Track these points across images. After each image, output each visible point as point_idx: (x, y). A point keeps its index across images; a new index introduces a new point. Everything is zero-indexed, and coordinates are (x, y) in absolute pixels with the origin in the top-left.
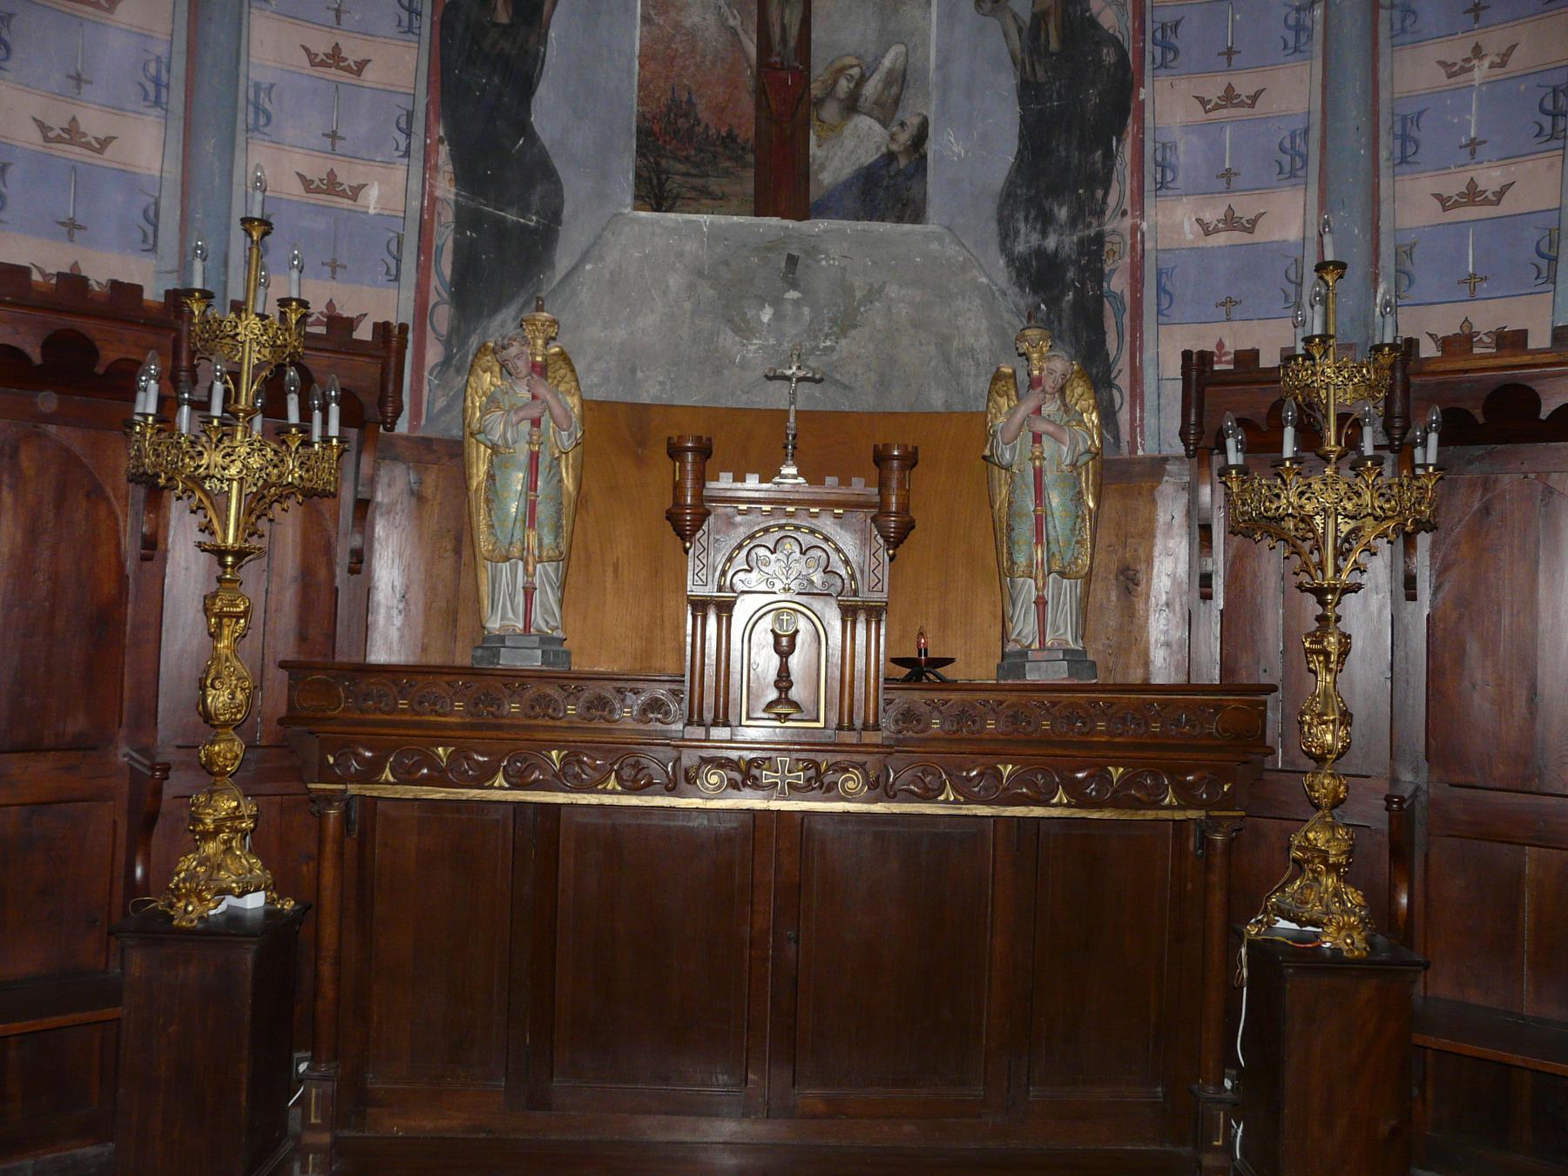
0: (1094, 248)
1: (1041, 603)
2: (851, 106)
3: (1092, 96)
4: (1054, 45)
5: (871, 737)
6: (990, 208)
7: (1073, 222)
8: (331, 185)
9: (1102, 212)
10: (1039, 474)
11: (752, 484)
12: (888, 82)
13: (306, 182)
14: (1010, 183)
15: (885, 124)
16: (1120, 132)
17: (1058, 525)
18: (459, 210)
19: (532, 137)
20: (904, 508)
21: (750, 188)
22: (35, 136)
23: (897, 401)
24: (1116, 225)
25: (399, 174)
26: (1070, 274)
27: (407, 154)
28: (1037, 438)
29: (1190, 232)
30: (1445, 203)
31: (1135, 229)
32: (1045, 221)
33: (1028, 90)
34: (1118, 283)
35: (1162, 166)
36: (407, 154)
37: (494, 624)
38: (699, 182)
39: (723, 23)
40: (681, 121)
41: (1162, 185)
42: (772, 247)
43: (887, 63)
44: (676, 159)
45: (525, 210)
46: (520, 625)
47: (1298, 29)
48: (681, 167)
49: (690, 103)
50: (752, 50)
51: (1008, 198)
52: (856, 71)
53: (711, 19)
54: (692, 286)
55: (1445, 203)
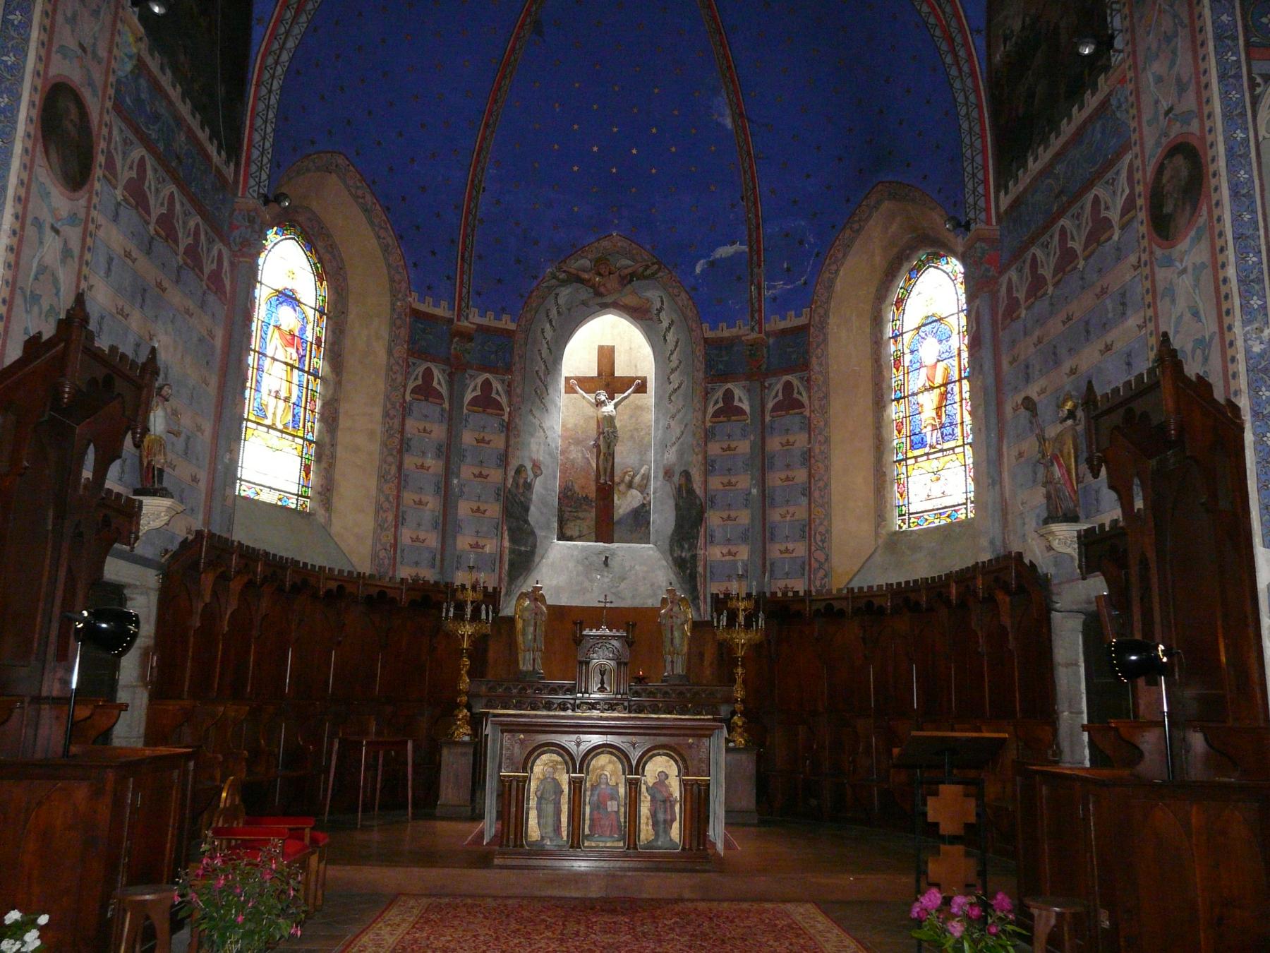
0: (694, 557)
1: (672, 662)
3: (694, 512)
4: (684, 495)
5: (624, 696)
6: (667, 542)
7: (689, 549)
8: (477, 546)
9: (696, 548)
10: (672, 627)
11: (594, 632)
12: (643, 479)
13: (471, 545)
14: (672, 534)
15: (642, 494)
16: (701, 525)
17: (677, 641)
18: (510, 548)
19: (529, 524)
20: (633, 637)
21: (593, 514)
22: (410, 541)
23: (637, 603)
25: (495, 541)
26: (689, 565)
27: (497, 535)
28: (672, 617)
29: (719, 555)
30: (781, 552)
31: (704, 554)
32: (682, 548)
34: (700, 569)
35: (712, 536)
36: (497, 535)
37: (522, 667)
38: (576, 514)
39: (584, 457)
40: (569, 493)
41: (712, 542)
42: (600, 553)
43: (642, 471)
44: (567, 506)
45: (525, 545)
46: (531, 669)
47: (747, 500)
48: (569, 509)
49: (572, 486)
50: (595, 466)
52: (631, 473)
53: (580, 455)
54: (575, 566)
55: (781, 552)
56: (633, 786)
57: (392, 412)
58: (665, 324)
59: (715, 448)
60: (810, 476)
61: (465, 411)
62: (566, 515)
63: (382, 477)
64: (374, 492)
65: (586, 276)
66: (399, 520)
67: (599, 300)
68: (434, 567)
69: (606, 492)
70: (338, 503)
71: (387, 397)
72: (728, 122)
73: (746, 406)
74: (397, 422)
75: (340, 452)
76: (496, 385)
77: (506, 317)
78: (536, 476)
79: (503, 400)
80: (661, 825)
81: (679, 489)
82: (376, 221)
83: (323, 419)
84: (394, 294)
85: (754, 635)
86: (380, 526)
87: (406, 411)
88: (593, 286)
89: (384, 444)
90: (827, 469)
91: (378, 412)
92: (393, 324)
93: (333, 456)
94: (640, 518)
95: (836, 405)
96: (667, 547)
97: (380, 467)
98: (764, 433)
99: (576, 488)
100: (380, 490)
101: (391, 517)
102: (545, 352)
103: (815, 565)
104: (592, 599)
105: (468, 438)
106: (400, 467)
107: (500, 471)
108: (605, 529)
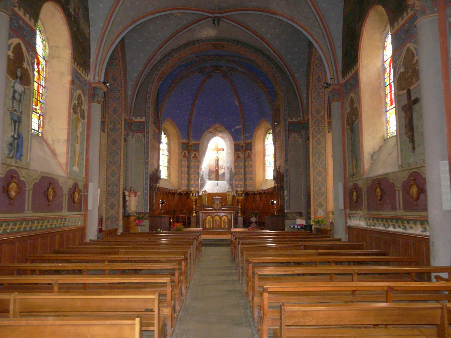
0: (233, 183)
2: (222, 168)
24: (234, 183)
33: (230, 174)
56: (221, 220)
62: (210, 174)
63: (178, 172)
66: (182, 180)
68: (50, 117)
69: (217, 171)
70: (171, 177)
71: (178, 158)
72: (237, 104)
73: (241, 156)
74: (180, 163)
75: (171, 168)
76: (197, 154)
77: (198, 141)
79: (198, 156)
80: (225, 225)
81: (230, 171)
83: (168, 163)
85: (242, 198)
87: (181, 160)
90: (255, 168)
91: (177, 161)
94: (224, 174)
95: (257, 157)
98: (245, 161)
100: (178, 174)
101: (180, 179)
102: (205, 146)
104: (215, 191)
105: (192, 164)
106: (181, 170)
108: (217, 178)
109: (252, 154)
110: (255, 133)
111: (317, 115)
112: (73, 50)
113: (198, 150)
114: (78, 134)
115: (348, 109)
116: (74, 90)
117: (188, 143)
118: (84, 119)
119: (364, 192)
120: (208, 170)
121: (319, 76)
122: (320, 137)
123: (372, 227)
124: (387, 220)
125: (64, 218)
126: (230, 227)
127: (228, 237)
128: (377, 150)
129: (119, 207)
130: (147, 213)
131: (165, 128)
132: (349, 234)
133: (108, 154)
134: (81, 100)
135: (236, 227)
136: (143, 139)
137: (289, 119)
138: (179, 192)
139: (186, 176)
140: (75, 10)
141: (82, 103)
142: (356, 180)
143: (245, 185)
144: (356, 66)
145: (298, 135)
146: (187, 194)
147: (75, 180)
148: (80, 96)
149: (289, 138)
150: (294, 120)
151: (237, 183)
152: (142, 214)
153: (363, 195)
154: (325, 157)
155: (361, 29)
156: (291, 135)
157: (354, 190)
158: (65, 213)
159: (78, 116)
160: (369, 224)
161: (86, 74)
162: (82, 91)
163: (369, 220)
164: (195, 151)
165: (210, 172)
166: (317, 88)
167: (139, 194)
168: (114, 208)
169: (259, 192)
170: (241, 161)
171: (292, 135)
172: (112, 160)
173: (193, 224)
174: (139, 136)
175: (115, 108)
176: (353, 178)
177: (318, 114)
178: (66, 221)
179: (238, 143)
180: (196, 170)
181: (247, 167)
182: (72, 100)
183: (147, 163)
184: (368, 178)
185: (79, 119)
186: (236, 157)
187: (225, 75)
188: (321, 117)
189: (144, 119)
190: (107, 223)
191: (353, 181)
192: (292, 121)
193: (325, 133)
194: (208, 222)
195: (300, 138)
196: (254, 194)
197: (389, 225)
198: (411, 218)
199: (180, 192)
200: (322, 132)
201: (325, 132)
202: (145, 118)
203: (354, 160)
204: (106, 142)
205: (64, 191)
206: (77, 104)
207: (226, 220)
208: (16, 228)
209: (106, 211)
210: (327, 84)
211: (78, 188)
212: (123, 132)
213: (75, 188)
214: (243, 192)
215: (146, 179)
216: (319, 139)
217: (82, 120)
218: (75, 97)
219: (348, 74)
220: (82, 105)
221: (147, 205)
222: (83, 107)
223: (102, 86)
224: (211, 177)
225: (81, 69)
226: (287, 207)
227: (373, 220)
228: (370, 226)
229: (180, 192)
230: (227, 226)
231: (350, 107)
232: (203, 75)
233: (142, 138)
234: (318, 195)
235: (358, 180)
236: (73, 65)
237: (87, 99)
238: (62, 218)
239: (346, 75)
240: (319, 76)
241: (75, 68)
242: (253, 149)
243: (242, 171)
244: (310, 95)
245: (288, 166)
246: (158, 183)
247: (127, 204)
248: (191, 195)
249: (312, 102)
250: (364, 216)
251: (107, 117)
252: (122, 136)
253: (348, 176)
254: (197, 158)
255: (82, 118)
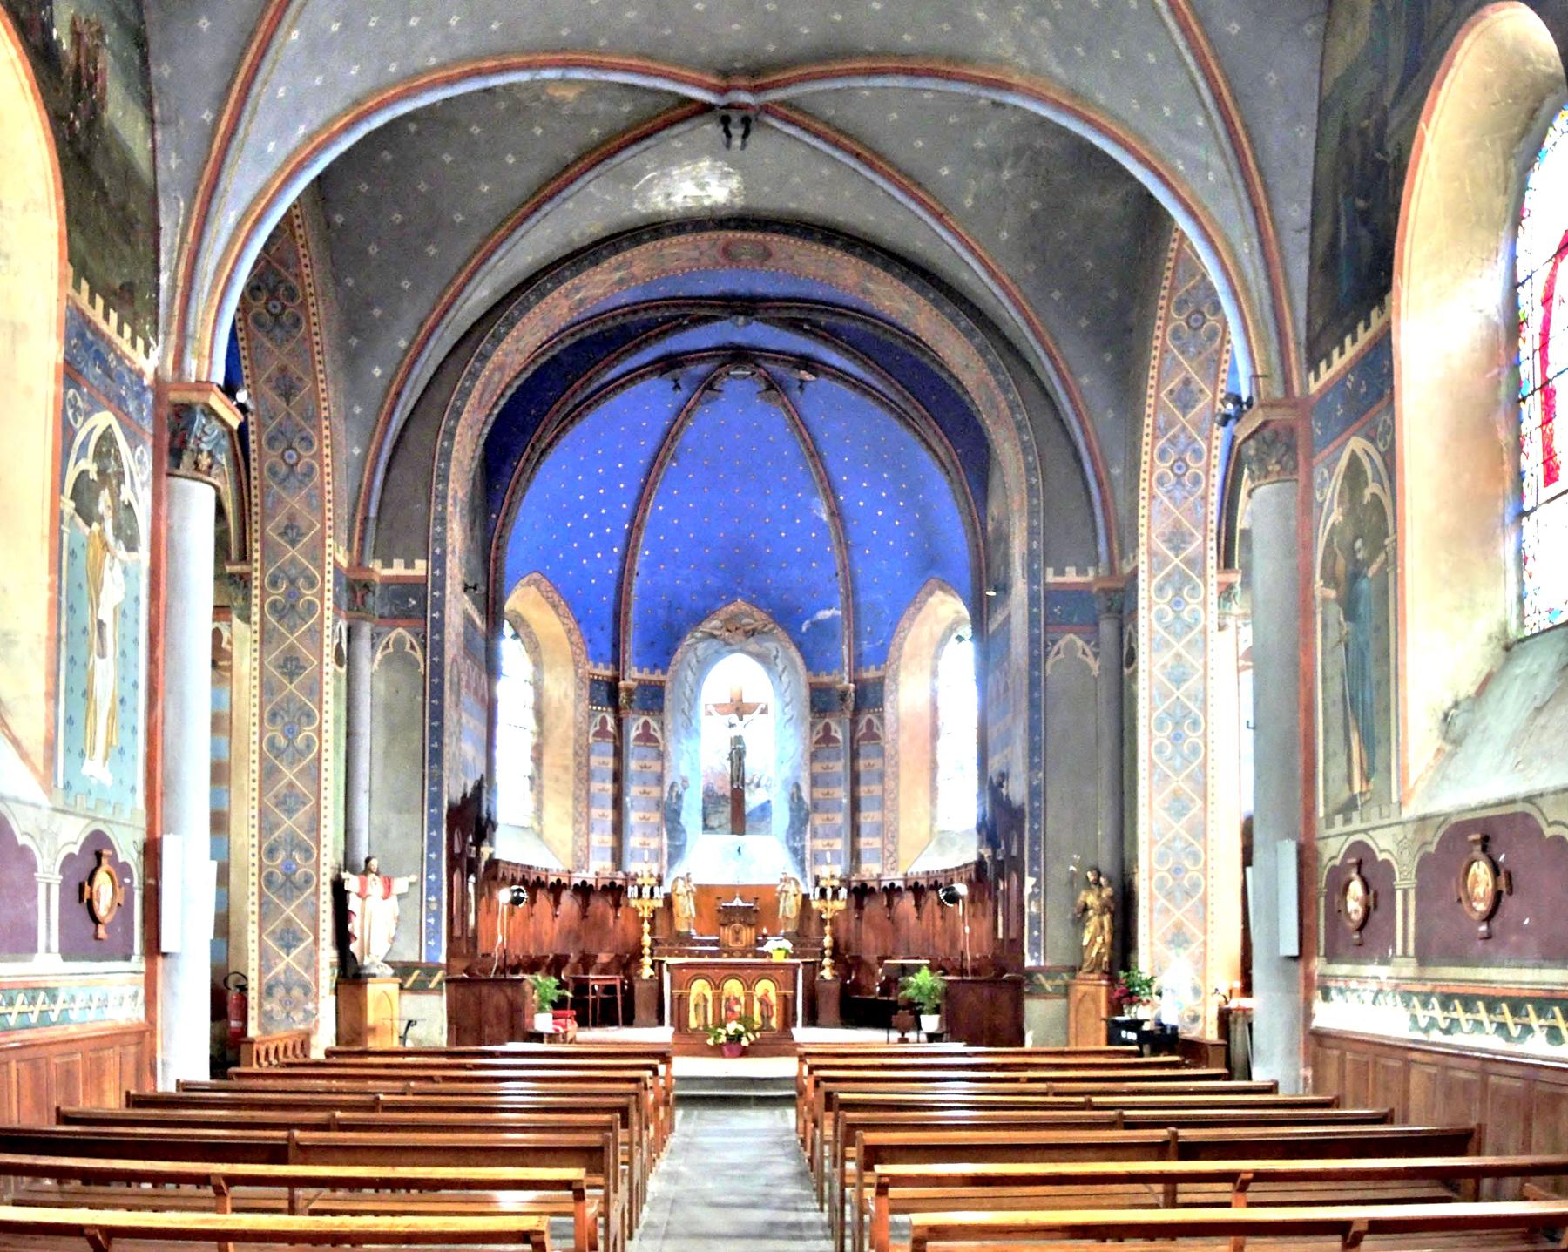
0: (803, 847)
2: (758, 785)
24: (808, 844)
32: (794, 839)
33: (791, 810)
51: (788, 832)
56: (749, 997)
57: (580, 752)
58: (780, 668)
59: (818, 768)
60: (884, 790)
61: (631, 746)
62: (709, 810)
63: (576, 799)
64: (571, 810)
65: (716, 633)
67: (728, 648)
69: (737, 798)
71: (576, 741)
72: (825, 517)
73: (840, 736)
74: (583, 760)
75: (546, 782)
76: (653, 724)
77: (659, 671)
78: (685, 788)
79: (658, 735)
80: (766, 1018)
82: (561, 612)
84: (576, 665)
86: (577, 833)
87: (589, 751)
88: (724, 640)
89: (576, 776)
90: (897, 785)
92: (577, 686)
93: (541, 786)
94: (765, 809)
96: (784, 839)
97: (574, 793)
99: (716, 788)
100: (575, 808)
101: (584, 827)
102: (688, 692)
103: (887, 854)
107: (659, 789)
109: (883, 725)
110: (897, 640)
111: (1171, 554)
112: (69, 222)
113: (661, 710)
114: (105, 614)
115: (1330, 511)
116: (76, 409)
117: (616, 679)
118: (131, 546)
119: (1405, 880)
120: (667, 704)
121: (1187, 382)
122: (1184, 652)
123: (1436, 1036)
124: (1517, 1006)
125: (46, 990)
126: (788, 1021)
127: (785, 1067)
128: (1472, 690)
129: (316, 941)
130: (439, 967)
131: (518, 615)
132: (1314, 1062)
133: (266, 716)
134: (118, 459)
135: (812, 1019)
136: (419, 656)
137: (1050, 571)
138: (578, 882)
139: (609, 813)
140: (77, 36)
141: (120, 475)
142: (1365, 831)
143: (855, 855)
144: (1382, 311)
145: (1088, 642)
146: (615, 892)
147: (95, 819)
148: (107, 437)
149: (1047, 654)
150: (1071, 576)
151: (820, 844)
152: (417, 972)
153: (1399, 895)
154: (1205, 735)
155: (1414, 132)
156: (1054, 642)
157: (1354, 875)
158: (46, 963)
159: (103, 530)
160: (1423, 1023)
161: (140, 342)
162: (117, 417)
163: (1425, 1005)
164: (647, 710)
165: (711, 800)
166: (1175, 436)
167: (400, 885)
168: (295, 946)
169: (911, 883)
170: (838, 754)
171: (1061, 643)
172: (282, 742)
173: (640, 1012)
174: (399, 642)
175: (292, 517)
176: (1347, 821)
177: (1177, 549)
178: (54, 999)
179: (825, 678)
180: (648, 789)
181: (863, 779)
182: (66, 454)
183: (437, 756)
184: (1423, 819)
185: (105, 545)
186: (815, 738)
187: (773, 385)
188: (1190, 562)
189: (420, 568)
190: (267, 1007)
191: (1349, 834)
192: (1060, 579)
193: (1204, 631)
194: (696, 1006)
195: (1096, 655)
196: (892, 891)
197: (1528, 1029)
198: (1527, 993)
199: (584, 882)
200: (1190, 627)
201: (1205, 627)
202: (423, 562)
203: (1355, 739)
204: (256, 664)
205: (40, 868)
206: (93, 475)
207: (773, 998)
208: (37, 1013)
209: (261, 957)
210: (1237, 400)
211: (113, 859)
212: (328, 623)
213: (99, 855)
214: (845, 882)
215: (434, 823)
216: (1178, 656)
217: (122, 553)
218: (84, 445)
219: (1336, 353)
220: (121, 481)
221: (439, 932)
222: (126, 494)
223: (217, 402)
224: (713, 822)
225: (114, 316)
226: (1035, 944)
227: (1445, 1005)
228: (1426, 1031)
229: (584, 882)
230: (774, 1023)
231: (1340, 503)
232: (677, 387)
233: (412, 647)
234: (1169, 895)
235: (1374, 829)
236: (71, 292)
237: (148, 458)
238: (32, 991)
239: (1328, 357)
240: (1187, 382)
241: (78, 309)
242: (887, 706)
243: (842, 795)
244: (1143, 467)
245: (1041, 775)
246: (491, 844)
247: (354, 926)
248: (632, 891)
249: (1153, 497)
250: (1397, 986)
251: (256, 556)
252: (327, 641)
253: (1321, 812)
254: (657, 741)
255: (121, 544)
